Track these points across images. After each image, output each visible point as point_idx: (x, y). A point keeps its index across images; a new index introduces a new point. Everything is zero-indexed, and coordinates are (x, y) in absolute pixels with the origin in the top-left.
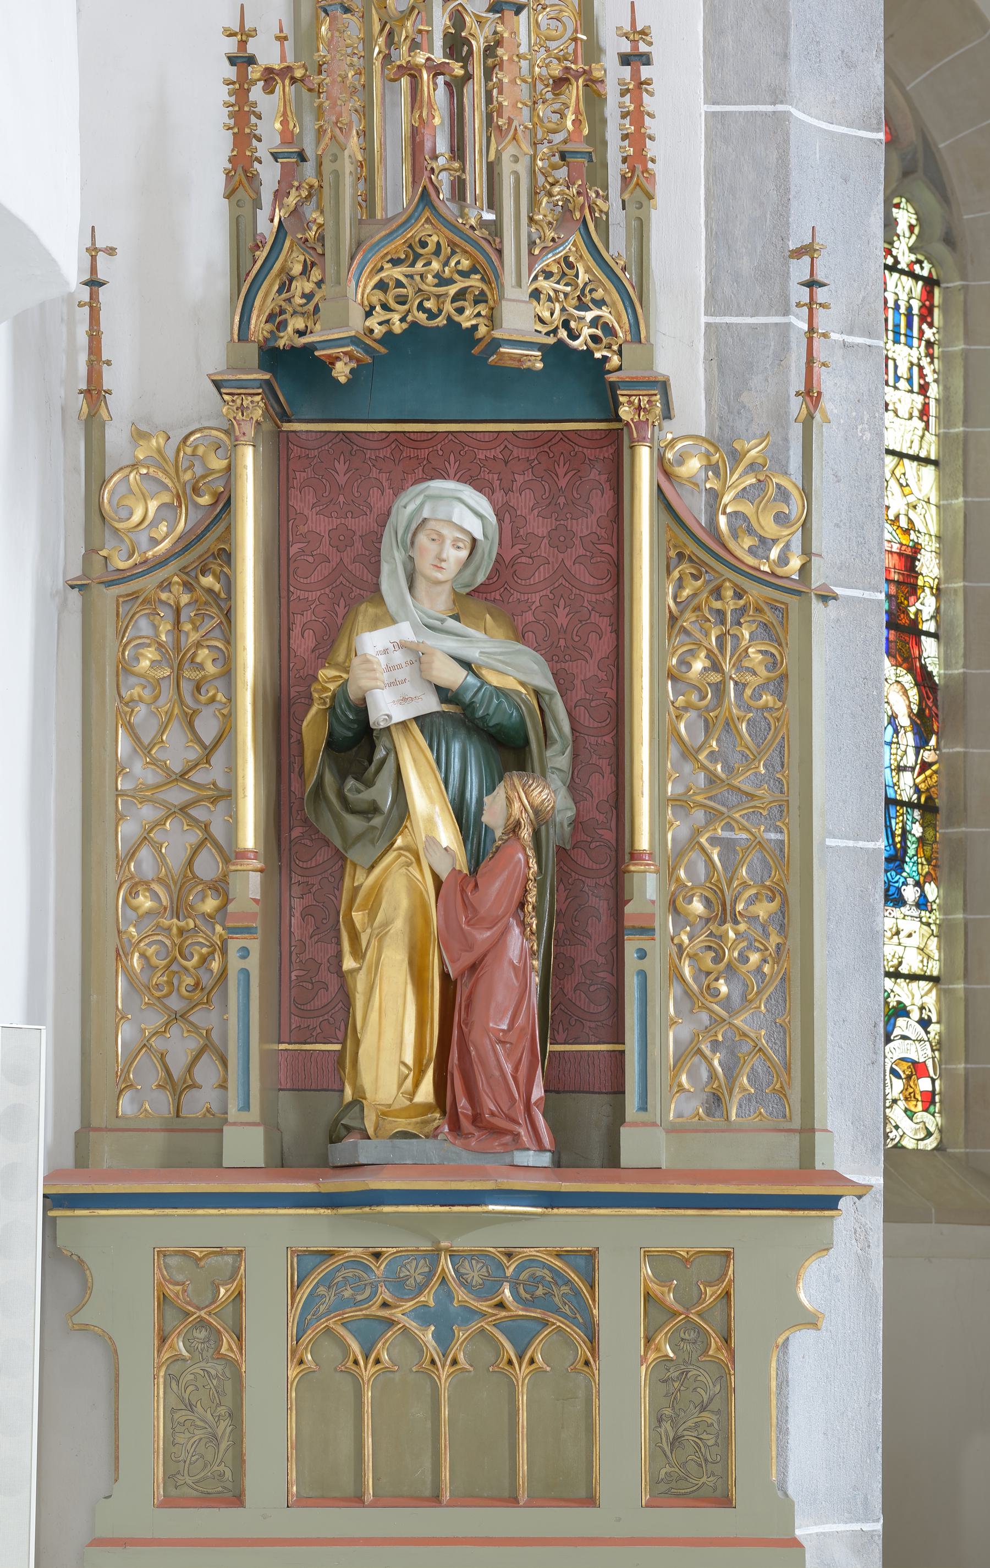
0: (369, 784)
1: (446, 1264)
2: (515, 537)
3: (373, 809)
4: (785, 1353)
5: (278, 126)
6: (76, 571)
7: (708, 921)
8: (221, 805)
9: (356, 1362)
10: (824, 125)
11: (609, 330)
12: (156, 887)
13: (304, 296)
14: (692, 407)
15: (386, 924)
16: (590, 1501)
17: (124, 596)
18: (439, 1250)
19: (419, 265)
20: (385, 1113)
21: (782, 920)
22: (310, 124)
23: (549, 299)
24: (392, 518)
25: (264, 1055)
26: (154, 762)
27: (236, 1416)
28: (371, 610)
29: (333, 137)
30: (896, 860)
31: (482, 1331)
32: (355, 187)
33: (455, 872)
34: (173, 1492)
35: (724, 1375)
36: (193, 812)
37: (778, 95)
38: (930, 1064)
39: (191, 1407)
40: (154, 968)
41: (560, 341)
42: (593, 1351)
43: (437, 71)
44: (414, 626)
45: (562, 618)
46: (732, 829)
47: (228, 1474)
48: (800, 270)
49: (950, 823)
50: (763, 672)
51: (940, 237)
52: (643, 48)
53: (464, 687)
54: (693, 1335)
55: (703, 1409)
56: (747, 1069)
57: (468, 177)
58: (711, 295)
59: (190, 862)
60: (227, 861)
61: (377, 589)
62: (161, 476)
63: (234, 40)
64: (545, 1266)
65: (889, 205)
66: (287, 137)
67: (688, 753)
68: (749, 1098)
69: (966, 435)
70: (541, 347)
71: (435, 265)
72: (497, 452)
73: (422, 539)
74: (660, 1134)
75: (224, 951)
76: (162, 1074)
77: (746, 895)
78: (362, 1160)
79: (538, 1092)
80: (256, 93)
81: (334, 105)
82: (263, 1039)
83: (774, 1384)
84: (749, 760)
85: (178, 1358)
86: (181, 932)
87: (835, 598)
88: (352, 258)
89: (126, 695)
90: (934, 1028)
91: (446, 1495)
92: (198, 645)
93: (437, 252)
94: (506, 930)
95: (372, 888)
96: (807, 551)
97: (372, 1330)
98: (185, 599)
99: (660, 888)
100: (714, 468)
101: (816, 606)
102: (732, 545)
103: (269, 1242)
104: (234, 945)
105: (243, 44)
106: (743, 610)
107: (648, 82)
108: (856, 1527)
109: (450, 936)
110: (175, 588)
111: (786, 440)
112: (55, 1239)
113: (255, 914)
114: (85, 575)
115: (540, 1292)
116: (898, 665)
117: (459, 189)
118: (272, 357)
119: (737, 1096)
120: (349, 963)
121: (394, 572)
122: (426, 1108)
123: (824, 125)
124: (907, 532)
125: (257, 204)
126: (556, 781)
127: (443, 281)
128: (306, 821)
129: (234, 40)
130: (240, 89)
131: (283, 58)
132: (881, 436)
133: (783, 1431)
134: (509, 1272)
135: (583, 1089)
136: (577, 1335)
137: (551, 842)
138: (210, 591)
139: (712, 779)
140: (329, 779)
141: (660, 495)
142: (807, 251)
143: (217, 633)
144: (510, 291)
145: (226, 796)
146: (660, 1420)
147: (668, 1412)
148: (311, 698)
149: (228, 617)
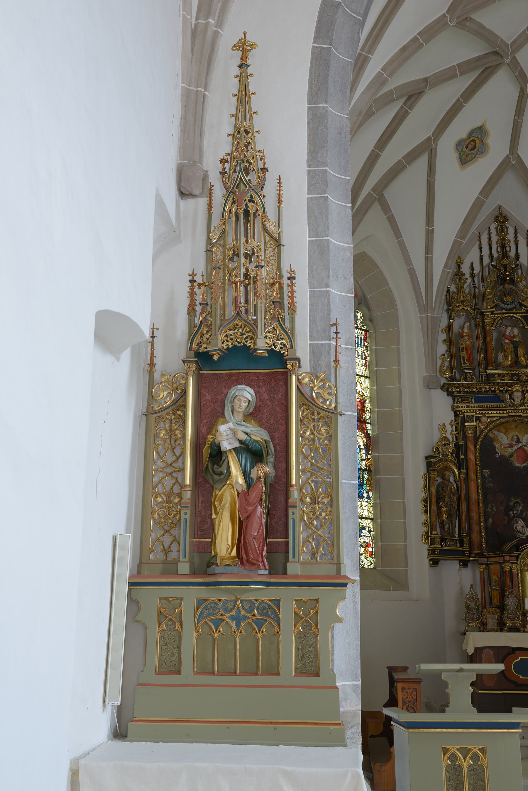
0: (220, 467)
1: (239, 603)
2: (260, 400)
3: (221, 473)
4: (333, 630)
5: (201, 297)
6: (145, 410)
7: (311, 504)
8: (181, 472)
9: (213, 632)
10: (339, 293)
11: (285, 346)
12: (162, 495)
13: (206, 339)
14: (306, 365)
15: (224, 505)
16: (279, 674)
17: (156, 417)
18: (237, 599)
19: (236, 330)
20: (223, 559)
21: (331, 504)
22: (209, 296)
23: (270, 338)
24: (228, 395)
25: (190, 542)
26: (163, 461)
27: (179, 648)
28: (222, 420)
29: (215, 299)
30: (361, 485)
31: (249, 623)
32: (220, 311)
33: (243, 491)
34: (161, 670)
35: (316, 636)
36: (173, 475)
37: (327, 286)
38: (371, 543)
39: (167, 645)
40: (161, 518)
41: (272, 349)
42: (279, 629)
43: (241, 282)
44: (233, 424)
45: (272, 421)
46: (317, 478)
47: (177, 665)
48: (333, 329)
49: (375, 475)
50: (325, 435)
51: (368, 320)
52: (293, 275)
53: (246, 440)
54: (307, 624)
55: (310, 647)
56: (322, 546)
57: (249, 308)
58: (310, 283)
59: (172, 488)
60: (182, 488)
61: (224, 413)
62: (168, 385)
63: (191, 277)
64: (266, 603)
65: (356, 312)
66: (204, 300)
67: (306, 457)
68: (323, 554)
69: (376, 370)
70: (267, 350)
71: (240, 330)
72: (255, 378)
73: (236, 401)
74: (298, 565)
75: (180, 513)
76: (162, 548)
77: (321, 497)
78: (216, 573)
79: (265, 553)
80: (196, 289)
81: (215, 291)
82: (190, 538)
83: (330, 639)
84: (322, 459)
85: (164, 630)
86: (169, 507)
87: (344, 414)
88: (219, 329)
89: (157, 443)
90: (372, 533)
91: (238, 672)
92: (176, 429)
93: (241, 327)
94: (257, 507)
95: (221, 495)
96: (336, 402)
97: (218, 622)
98: (173, 417)
99: (298, 495)
100: (312, 381)
101: (339, 417)
102: (317, 401)
103: (190, 596)
104: (183, 511)
105: (193, 277)
106: (320, 418)
107: (295, 284)
108: (354, 683)
109: (242, 509)
110: (170, 415)
111: (330, 373)
112: (131, 595)
113: (188, 503)
114: (147, 411)
115: (265, 611)
116: (360, 432)
117: (247, 311)
118: (198, 354)
119: (319, 554)
120: (214, 516)
121: (228, 409)
122: (234, 557)
123: (339, 293)
124: (362, 396)
125: (195, 316)
126: (270, 465)
127: (242, 334)
128: (203, 477)
129: (191, 277)
130: (192, 288)
131: (203, 280)
132: (355, 371)
133: (333, 653)
134: (256, 605)
135: (277, 554)
136: (275, 624)
137: (269, 482)
138: (180, 415)
139: (312, 464)
140: (210, 465)
141: (298, 388)
142: (335, 324)
143: (181, 426)
144: (259, 336)
145: (182, 470)
146: (298, 650)
147: (300, 647)
148: (205, 443)
149: (184, 422)
